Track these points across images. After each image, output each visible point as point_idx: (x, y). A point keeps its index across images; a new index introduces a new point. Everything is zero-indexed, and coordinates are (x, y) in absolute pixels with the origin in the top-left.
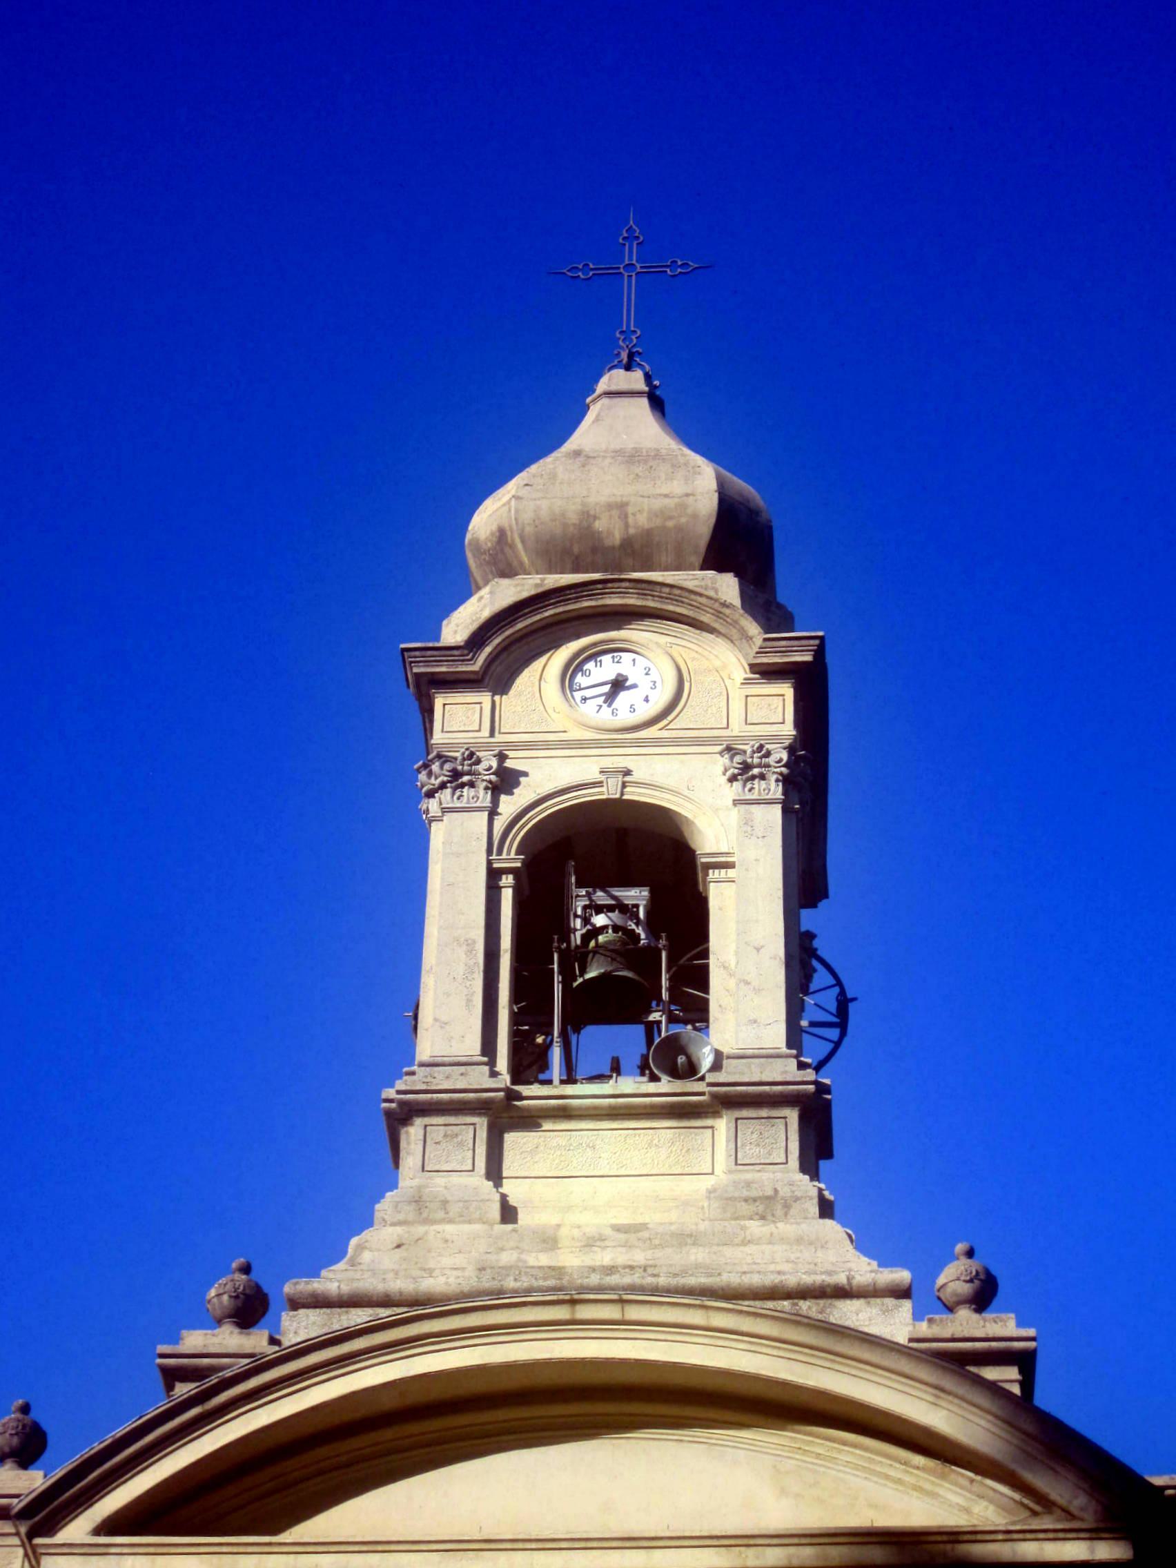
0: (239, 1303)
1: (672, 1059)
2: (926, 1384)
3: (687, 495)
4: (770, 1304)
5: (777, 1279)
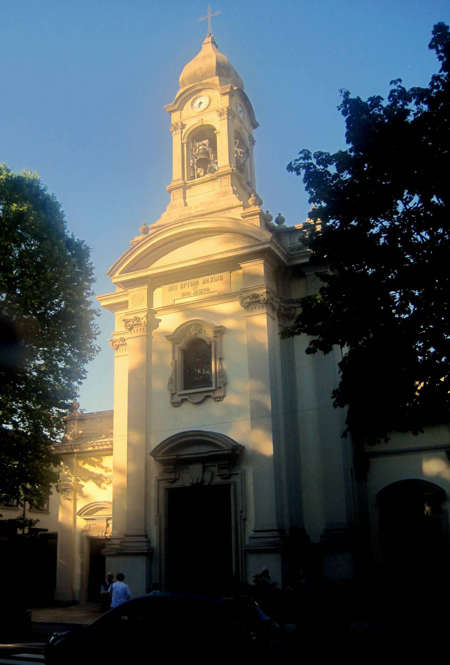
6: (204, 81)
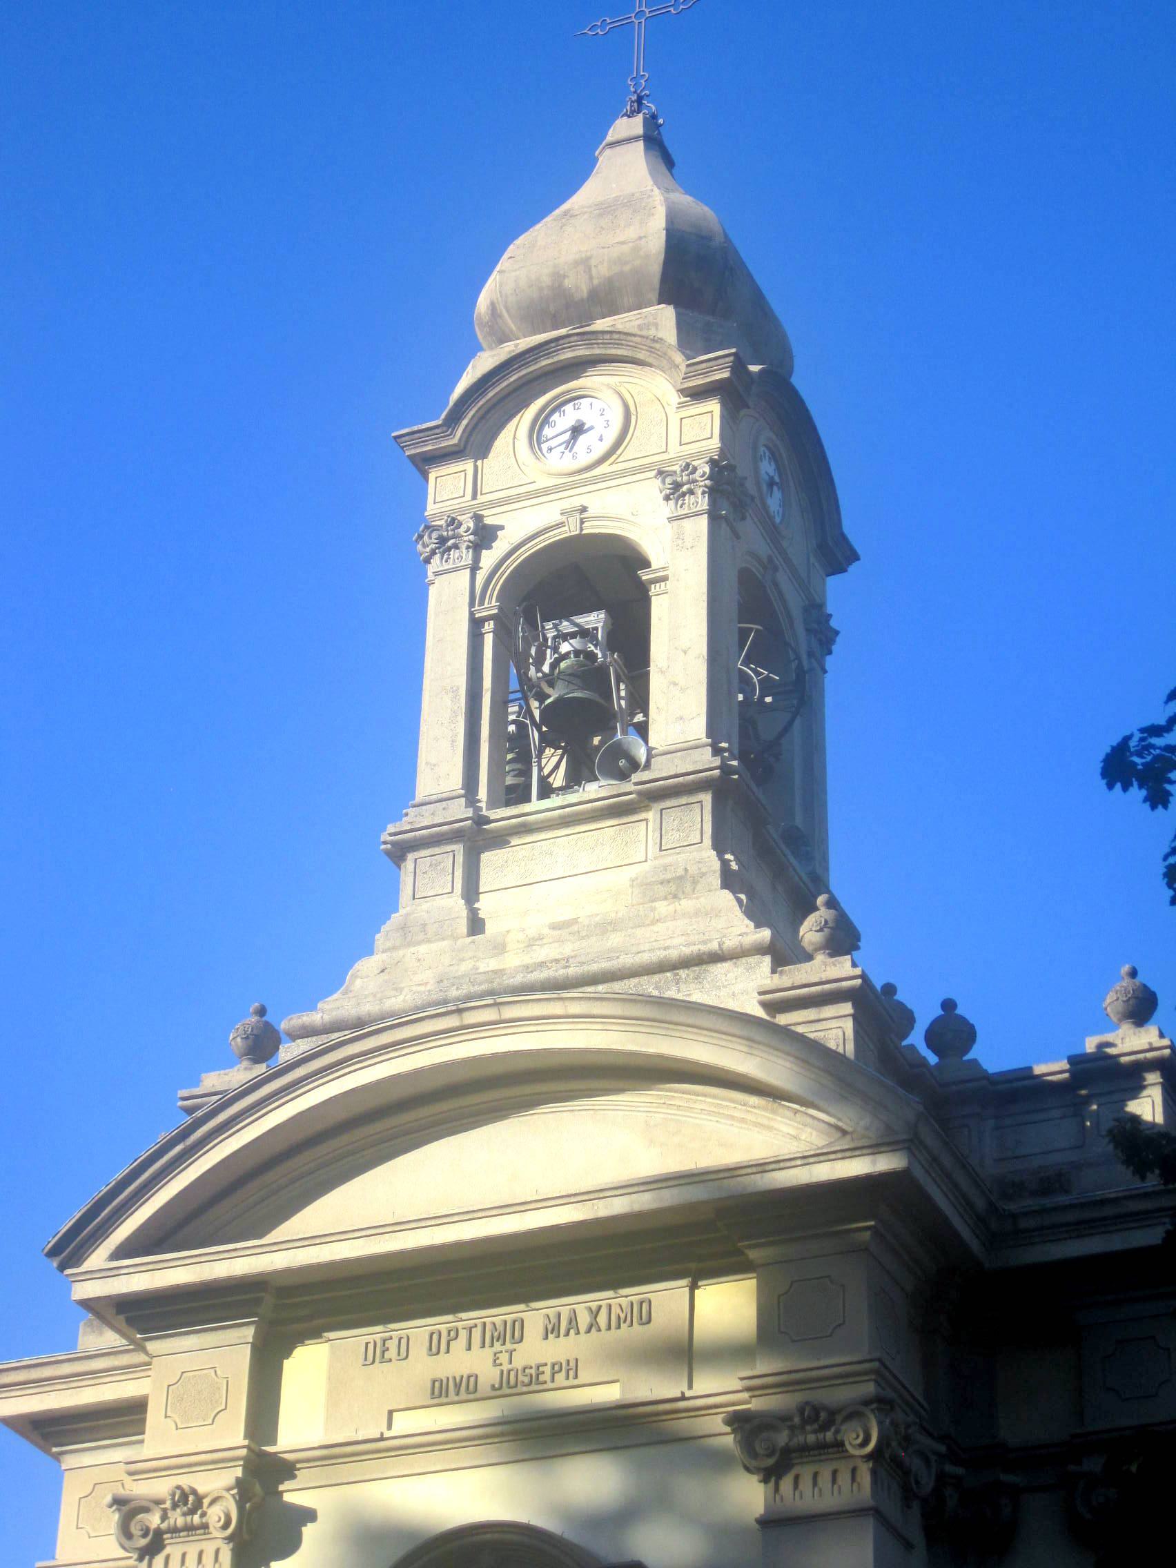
0: (250, 1042)
1: (620, 765)
2: (739, 1037)
3: (640, 238)
4: (600, 988)
5: (661, 954)
6: (600, 324)
